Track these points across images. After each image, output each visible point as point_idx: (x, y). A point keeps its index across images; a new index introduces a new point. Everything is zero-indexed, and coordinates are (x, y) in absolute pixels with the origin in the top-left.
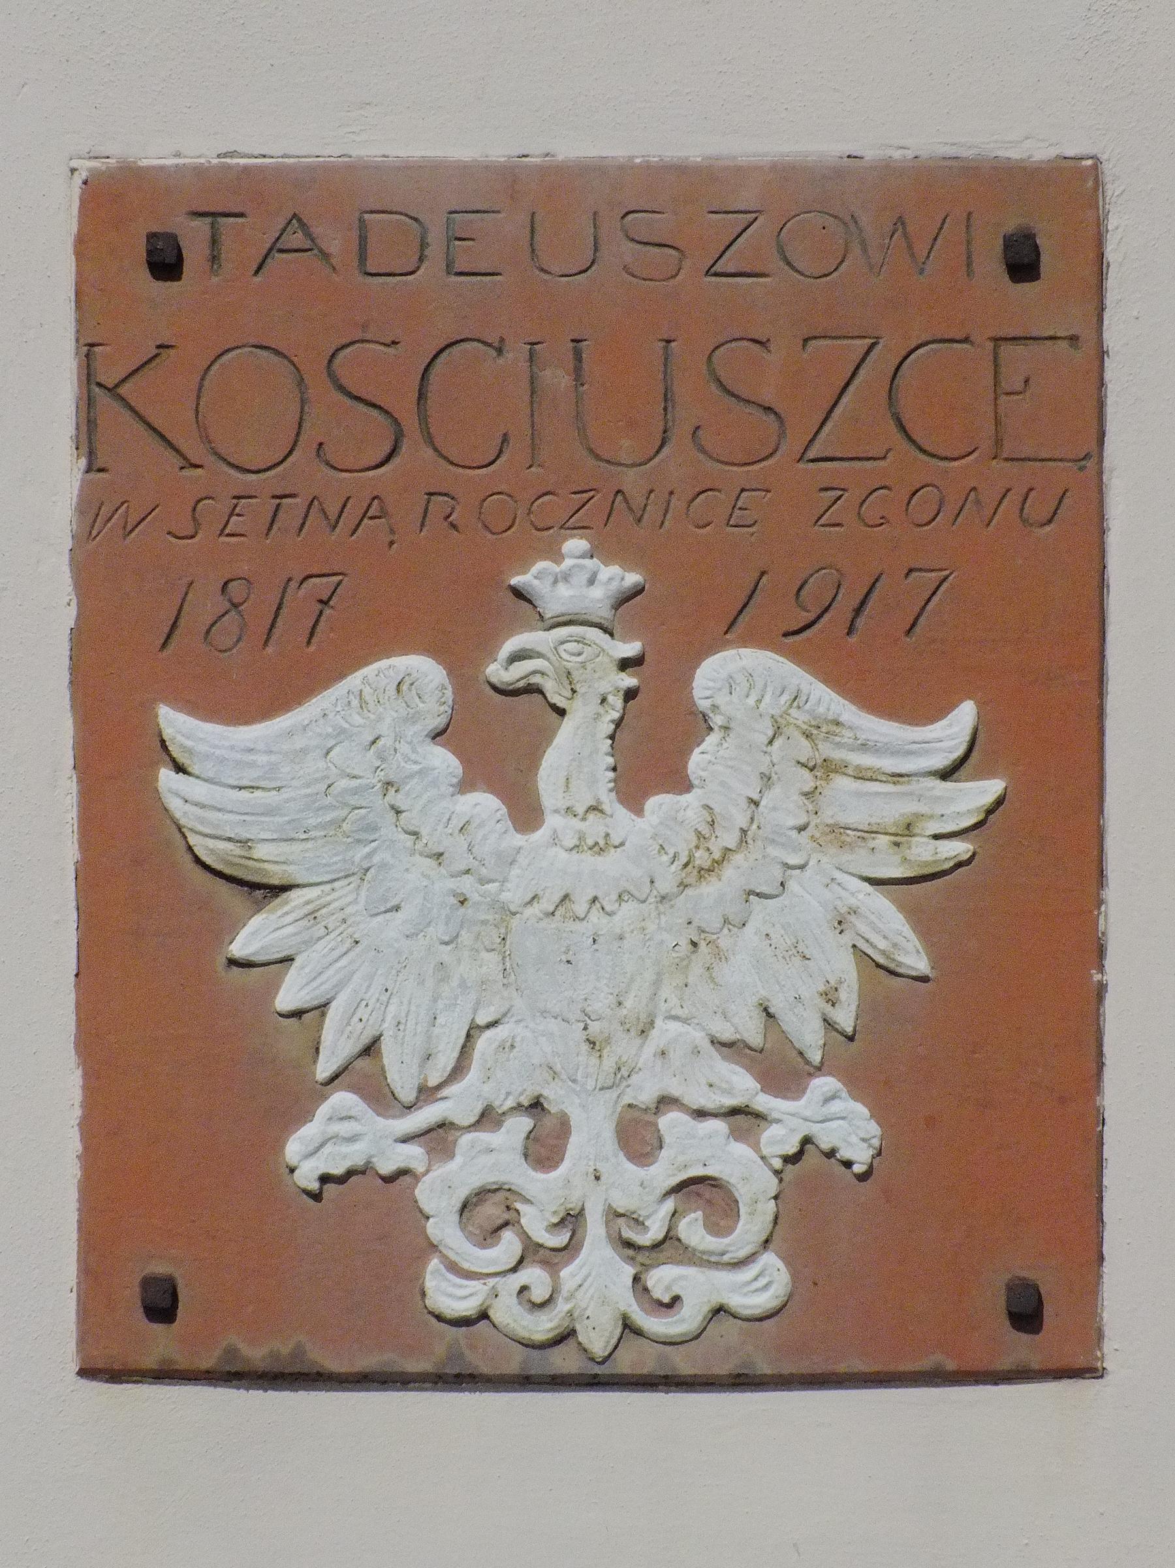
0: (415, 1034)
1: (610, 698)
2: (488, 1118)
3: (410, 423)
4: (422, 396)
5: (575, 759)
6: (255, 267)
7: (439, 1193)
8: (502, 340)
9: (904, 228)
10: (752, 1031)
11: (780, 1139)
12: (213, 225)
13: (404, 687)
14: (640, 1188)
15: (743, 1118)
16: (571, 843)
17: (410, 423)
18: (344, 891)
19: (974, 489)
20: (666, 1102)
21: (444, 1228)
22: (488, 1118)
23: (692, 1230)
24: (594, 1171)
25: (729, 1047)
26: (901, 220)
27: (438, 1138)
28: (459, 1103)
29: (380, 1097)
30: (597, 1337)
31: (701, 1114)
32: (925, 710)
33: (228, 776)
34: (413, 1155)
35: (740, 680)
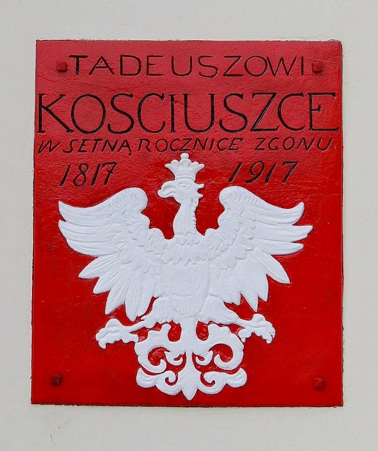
0: (135, 300)
1: (194, 200)
2: (158, 326)
3: (136, 118)
4: (139, 111)
5: (185, 220)
6: (226, 55)
7: (142, 350)
8: (163, 94)
9: (283, 61)
10: (238, 302)
11: (245, 334)
12: (77, 59)
13: (133, 196)
14: (203, 348)
15: (234, 328)
16: (182, 243)
17: (136, 118)
18: (116, 256)
19: (304, 138)
20: (210, 322)
21: (143, 360)
22: (158, 326)
23: (218, 361)
24: (189, 342)
25: (230, 306)
26: (282, 59)
27: (143, 333)
28: (148, 322)
29: (126, 321)
30: (190, 395)
31: (220, 325)
32: (288, 204)
33: (78, 226)
34: (135, 338)
35: (234, 197)
